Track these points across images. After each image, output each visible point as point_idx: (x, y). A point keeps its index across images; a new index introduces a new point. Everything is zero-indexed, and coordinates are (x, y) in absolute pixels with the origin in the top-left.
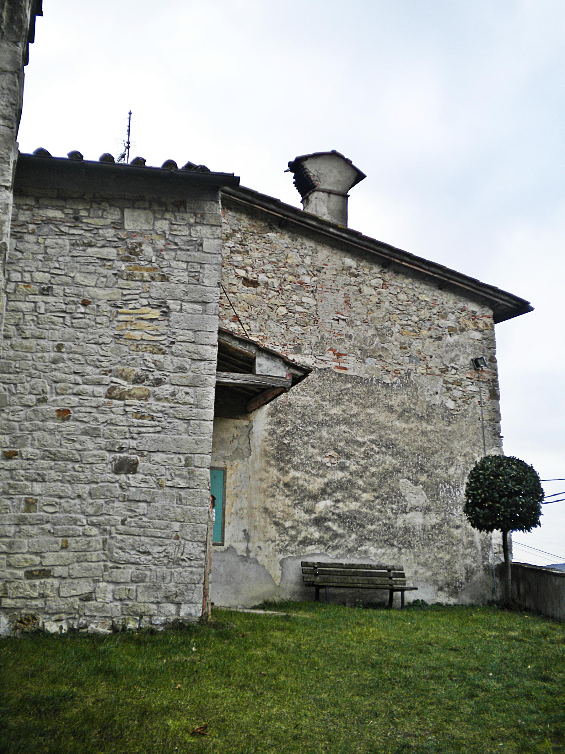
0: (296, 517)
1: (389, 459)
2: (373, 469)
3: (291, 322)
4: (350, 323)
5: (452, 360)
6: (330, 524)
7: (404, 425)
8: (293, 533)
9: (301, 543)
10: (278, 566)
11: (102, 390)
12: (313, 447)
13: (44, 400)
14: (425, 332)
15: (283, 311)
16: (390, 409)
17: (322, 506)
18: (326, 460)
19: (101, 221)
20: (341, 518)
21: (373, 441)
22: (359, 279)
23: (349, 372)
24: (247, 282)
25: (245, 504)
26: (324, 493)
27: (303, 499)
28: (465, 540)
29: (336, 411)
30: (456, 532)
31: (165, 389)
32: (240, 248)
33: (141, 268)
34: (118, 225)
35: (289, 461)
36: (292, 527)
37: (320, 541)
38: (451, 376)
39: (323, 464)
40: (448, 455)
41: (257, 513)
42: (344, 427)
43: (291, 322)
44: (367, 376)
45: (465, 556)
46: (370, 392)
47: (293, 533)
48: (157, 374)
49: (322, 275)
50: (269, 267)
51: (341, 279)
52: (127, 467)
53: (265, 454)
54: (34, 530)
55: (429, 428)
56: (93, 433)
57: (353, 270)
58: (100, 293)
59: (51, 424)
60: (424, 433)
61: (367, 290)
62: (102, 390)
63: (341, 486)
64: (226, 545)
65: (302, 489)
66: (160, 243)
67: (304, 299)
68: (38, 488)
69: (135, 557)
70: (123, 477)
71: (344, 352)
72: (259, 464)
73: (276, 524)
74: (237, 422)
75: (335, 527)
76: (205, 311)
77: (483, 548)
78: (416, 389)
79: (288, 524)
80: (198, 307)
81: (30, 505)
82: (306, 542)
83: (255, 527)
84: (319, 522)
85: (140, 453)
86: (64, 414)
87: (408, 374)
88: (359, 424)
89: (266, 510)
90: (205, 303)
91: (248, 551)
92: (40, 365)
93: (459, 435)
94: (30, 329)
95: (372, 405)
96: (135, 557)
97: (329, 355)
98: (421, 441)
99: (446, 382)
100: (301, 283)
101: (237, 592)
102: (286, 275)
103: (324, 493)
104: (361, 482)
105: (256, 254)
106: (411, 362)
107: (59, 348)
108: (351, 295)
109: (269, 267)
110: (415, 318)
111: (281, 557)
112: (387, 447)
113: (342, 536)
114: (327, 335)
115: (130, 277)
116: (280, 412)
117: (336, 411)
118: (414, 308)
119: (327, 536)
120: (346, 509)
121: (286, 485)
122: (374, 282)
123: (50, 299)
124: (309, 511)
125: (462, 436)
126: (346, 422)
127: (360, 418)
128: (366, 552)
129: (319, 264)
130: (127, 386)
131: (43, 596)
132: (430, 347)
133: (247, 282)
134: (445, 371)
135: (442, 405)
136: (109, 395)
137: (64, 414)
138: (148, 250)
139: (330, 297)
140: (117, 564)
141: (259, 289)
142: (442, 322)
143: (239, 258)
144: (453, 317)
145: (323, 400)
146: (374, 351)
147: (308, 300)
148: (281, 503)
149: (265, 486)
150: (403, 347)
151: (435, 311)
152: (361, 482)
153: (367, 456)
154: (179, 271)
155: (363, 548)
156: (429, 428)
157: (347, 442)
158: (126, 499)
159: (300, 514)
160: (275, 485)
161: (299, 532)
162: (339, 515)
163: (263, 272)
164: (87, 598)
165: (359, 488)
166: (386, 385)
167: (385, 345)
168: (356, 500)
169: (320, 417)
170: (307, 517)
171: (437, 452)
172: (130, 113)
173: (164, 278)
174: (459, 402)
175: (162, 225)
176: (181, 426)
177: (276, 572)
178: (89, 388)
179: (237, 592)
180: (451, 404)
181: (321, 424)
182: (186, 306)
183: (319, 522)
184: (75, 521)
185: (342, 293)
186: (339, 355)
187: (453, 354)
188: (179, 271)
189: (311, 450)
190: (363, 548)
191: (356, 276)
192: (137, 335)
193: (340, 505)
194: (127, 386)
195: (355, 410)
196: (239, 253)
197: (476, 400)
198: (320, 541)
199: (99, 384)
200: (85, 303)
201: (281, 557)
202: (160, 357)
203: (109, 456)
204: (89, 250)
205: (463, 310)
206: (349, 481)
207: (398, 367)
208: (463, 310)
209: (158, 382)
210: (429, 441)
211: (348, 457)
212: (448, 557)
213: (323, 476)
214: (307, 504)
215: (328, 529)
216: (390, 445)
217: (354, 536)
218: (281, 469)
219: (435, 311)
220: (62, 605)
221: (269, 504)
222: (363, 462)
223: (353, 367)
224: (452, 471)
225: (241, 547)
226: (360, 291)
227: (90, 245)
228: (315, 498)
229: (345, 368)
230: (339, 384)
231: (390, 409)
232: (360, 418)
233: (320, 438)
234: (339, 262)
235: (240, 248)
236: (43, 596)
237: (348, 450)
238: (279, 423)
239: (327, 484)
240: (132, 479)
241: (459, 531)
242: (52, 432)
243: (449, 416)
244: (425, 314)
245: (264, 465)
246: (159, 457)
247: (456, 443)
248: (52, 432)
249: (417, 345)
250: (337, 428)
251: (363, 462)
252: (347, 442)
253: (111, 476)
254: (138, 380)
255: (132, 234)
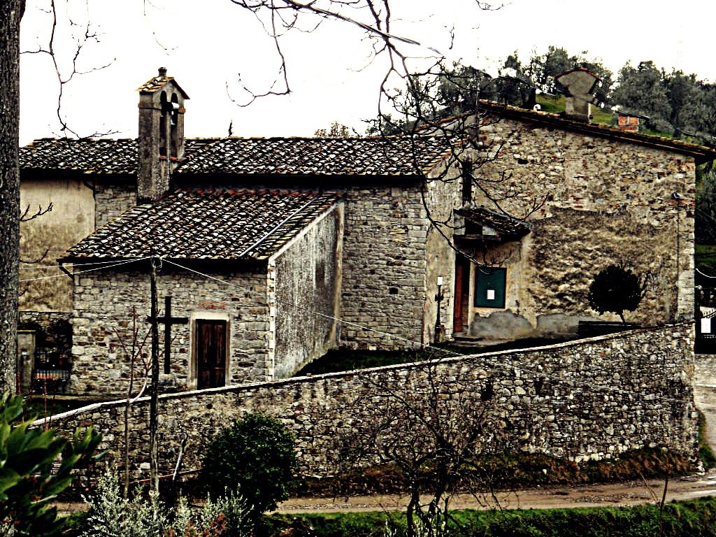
0: (547, 293)
1: (608, 259)
2: (596, 266)
3: (547, 182)
4: (586, 178)
5: (659, 195)
6: (567, 297)
7: (620, 238)
8: (544, 302)
9: (549, 307)
10: (535, 320)
11: (385, 262)
12: (558, 254)
13: (365, 267)
14: (640, 178)
15: (542, 176)
16: (611, 229)
17: (562, 287)
18: (566, 262)
19: (382, 195)
20: (574, 294)
21: (598, 249)
22: (594, 150)
23: (584, 209)
24: (522, 162)
25: (517, 287)
26: (564, 280)
27: (551, 284)
28: (658, 306)
29: (574, 233)
30: (652, 302)
31: (407, 261)
32: (516, 141)
33: (397, 212)
34: (389, 195)
35: (543, 263)
36: (544, 299)
37: (561, 307)
38: (656, 206)
39: (564, 264)
40: (650, 255)
41: (524, 292)
42: (579, 242)
43: (547, 182)
44: (596, 210)
45: (657, 316)
46: (597, 220)
47: (544, 302)
48: (404, 255)
49: (569, 151)
50: (534, 150)
51: (581, 152)
52: (394, 291)
53: (529, 259)
54: (365, 314)
55: (638, 239)
56: (382, 278)
57: (591, 144)
58: (383, 223)
59: (369, 276)
60: (634, 243)
61: (598, 156)
62: (385, 262)
63: (575, 276)
64: (506, 308)
65: (550, 278)
66: (405, 201)
67: (556, 167)
68: (365, 299)
69: (397, 324)
70: (393, 295)
71: (581, 197)
72: (526, 265)
73: (535, 297)
74: (513, 243)
75: (570, 299)
76: (421, 229)
77: (671, 311)
78: (630, 216)
79: (542, 297)
80: (419, 228)
81: (363, 305)
82: (552, 307)
83: (522, 299)
84: (561, 296)
85: (399, 286)
86: (372, 272)
87: (624, 207)
88: (589, 240)
89: (529, 290)
90: (421, 226)
91: (518, 311)
92: (364, 253)
93: (659, 242)
94: (361, 239)
95: (598, 228)
96: (397, 324)
97: (571, 200)
98: (631, 247)
99: (652, 209)
100: (555, 157)
101: (512, 332)
102: (545, 154)
103: (564, 280)
104: (588, 273)
105: (526, 144)
106: (628, 198)
107: (370, 246)
108: (587, 160)
109: (534, 150)
110: (633, 170)
111: (537, 314)
112: (607, 252)
113: (574, 304)
114: (570, 188)
115: (394, 216)
116: (539, 235)
117: (574, 233)
118: (633, 163)
119: (565, 304)
120: (577, 289)
121: (541, 276)
122: (604, 150)
123: (367, 227)
124: (554, 290)
125: (662, 243)
126: (581, 239)
127: (591, 235)
128: (589, 313)
129: (566, 144)
130: (393, 260)
131: (368, 337)
132: (643, 188)
133: (522, 162)
134: (653, 202)
135: (649, 224)
136: (387, 264)
137: (372, 272)
138: (400, 204)
139: (573, 164)
140: (393, 327)
141: (528, 165)
142: (654, 170)
143: (515, 148)
144: (662, 165)
145: (566, 226)
146: (602, 194)
147: (559, 167)
148: (537, 286)
149: (528, 277)
150: (622, 189)
151: (648, 163)
152: (588, 273)
153: (593, 258)
154: (412, 214)
155: (587, 311)
156: (638, 239)
157: (580, 251)
158: (394, 303)
159: (549, 292)
160: (535, 276)
161: (548, 302)
162: (572, 292)
163: (531, 154)
164: (382, 339)
165: (587, 277)
166: (608, 215)
167: (610, 190)
168: (585, 283)
169: (564, 237)
170: (553, 293)
171: (642, 254)
172: (431, 48)
173: (406, 216)
174: (662, 221)
175: (405, 193)
176: (413, 275)
177: (534, 323)
178: (380, 261)
179: (512, 332)
180: (655, 223)
181: (564, 241)
182: (414, 227)
183: (561, 296)
184: (378, 311)
185: (581, 160)
186: (578, 199)
187: (660, 191)
188: (412, 214)
189: (557, 256)
190: (587, 311)
191: (591, 148)
192: (397, 240)
193: (574, 287)
194: (393, 260)
195: (587, 231)
196: (516, 144)
197: (675, 220)
198: (561, 307)
199: (384, 259)
200: (379, 228)
201: (537, 314)
202: (404, 249)
203: (388, 287)
204: (380, 206)
205: (671, 159)
206: (580, 273)
207: (618, 202)
208: (671, 159)
209: (404, 259)
210: (637, 247)
211: (580, 259)
212: (644, 316)
213: (564, 271)
214: (553, 286)
215: (566, 300)
216: (609, 251)
217: (582, 304)
218: (538, 268)
219: (648, 163)
220: (374, 340)
221: (531, 286)
222: (590, 262)
223: (586, 205)
224: (652, 265)
225: (514, 309)
226: (594, 157)
227: (380, 204)
228: (558, 283)
229: (581, 207)
230: (577, 217)
231: (611, 229)
232: (589, 236)
233: (563, 249)
234: (580, 141)
235: (516, 141)
236: (368, 337)
237: (581, 255)
238: (538, 242)
239: (566, 275)
240: (396, 296)
241: (654, 301)
242: (369, 278)
243: (653, 231)
244: (641, 165)
245: (528, 265)
246: (405, 288)
247: (657, 247)
248: (369, 278)
249: (633, 187)
250: (575, 243)
251: (590, 262)
252: (580, 251)
253: (389, 295)
254: (398, 258)
255: (394, 198)
